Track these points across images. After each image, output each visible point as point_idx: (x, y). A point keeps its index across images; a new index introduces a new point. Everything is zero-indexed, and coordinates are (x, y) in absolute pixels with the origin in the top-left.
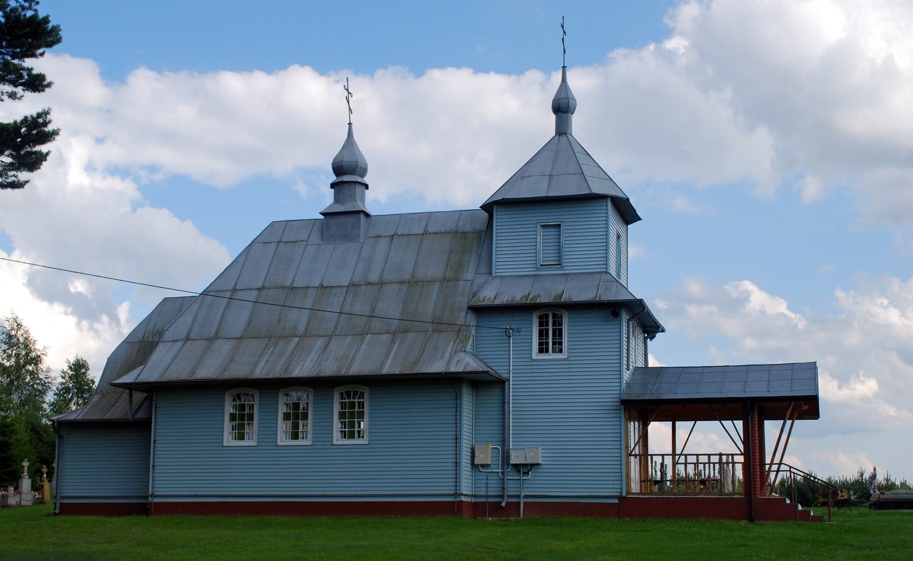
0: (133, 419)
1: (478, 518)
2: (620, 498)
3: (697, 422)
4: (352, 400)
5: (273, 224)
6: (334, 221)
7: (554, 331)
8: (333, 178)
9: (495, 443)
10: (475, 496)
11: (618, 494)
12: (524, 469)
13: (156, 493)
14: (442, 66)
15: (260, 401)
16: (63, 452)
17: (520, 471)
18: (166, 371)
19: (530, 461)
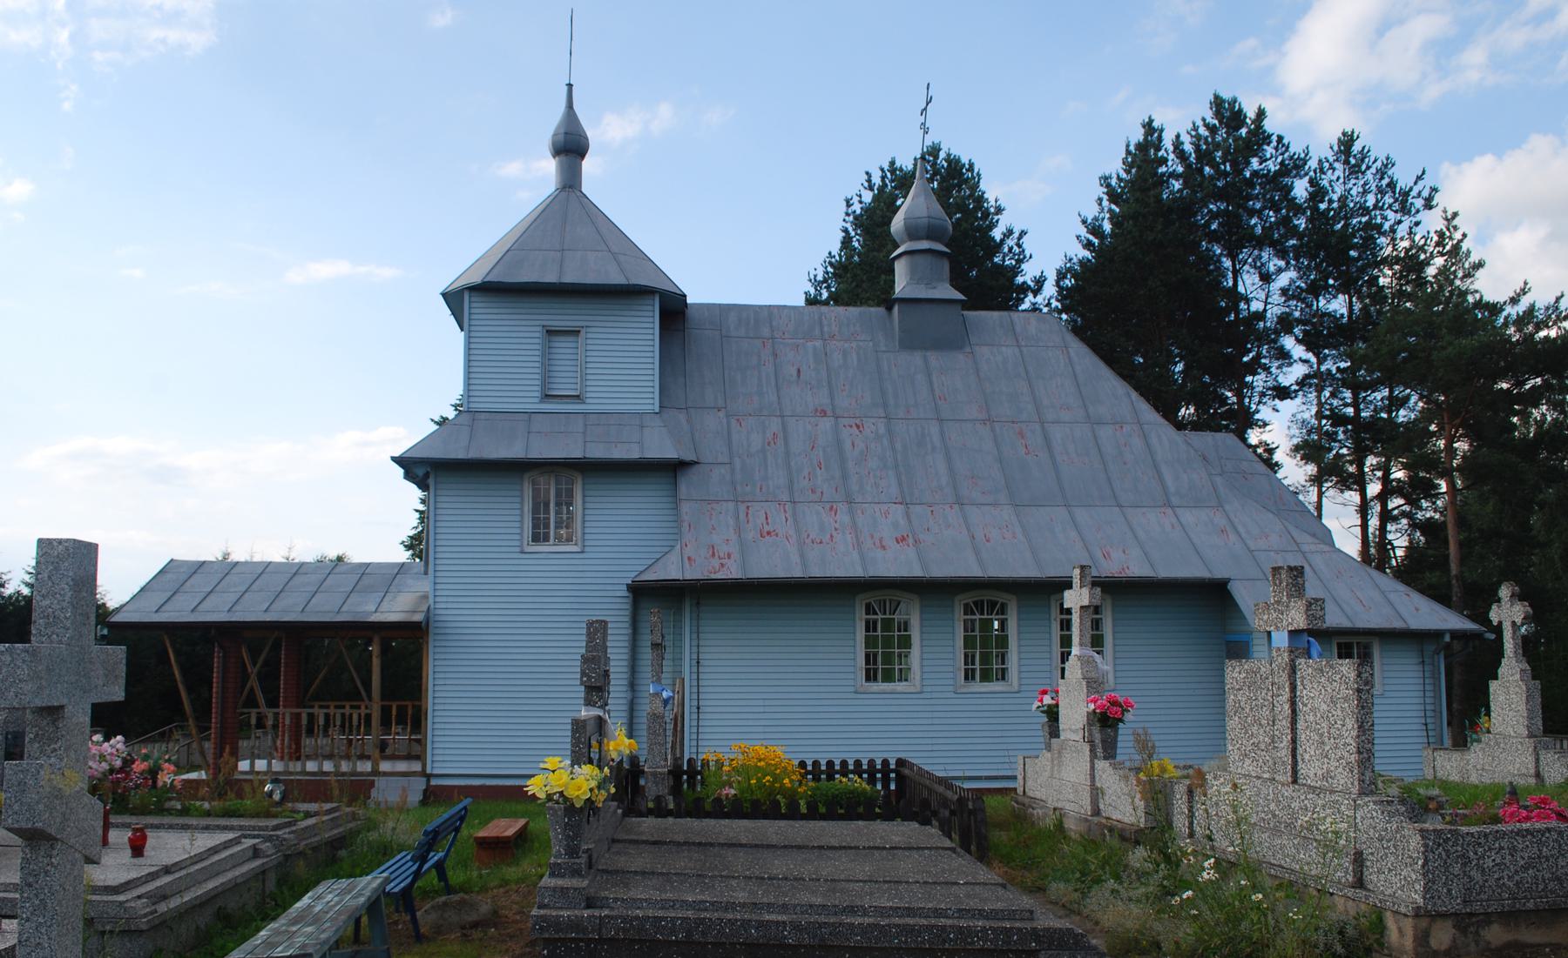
4: (985, 617)
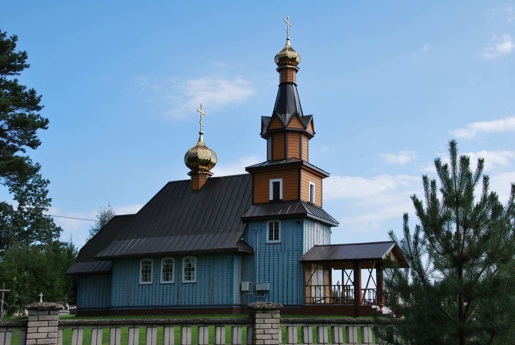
4: (168, 264)
5: (170, 184)
7: (275, 230)
12: (263, 293)
15: (197, 262)
18: (177, 244)
19: (264, 289)
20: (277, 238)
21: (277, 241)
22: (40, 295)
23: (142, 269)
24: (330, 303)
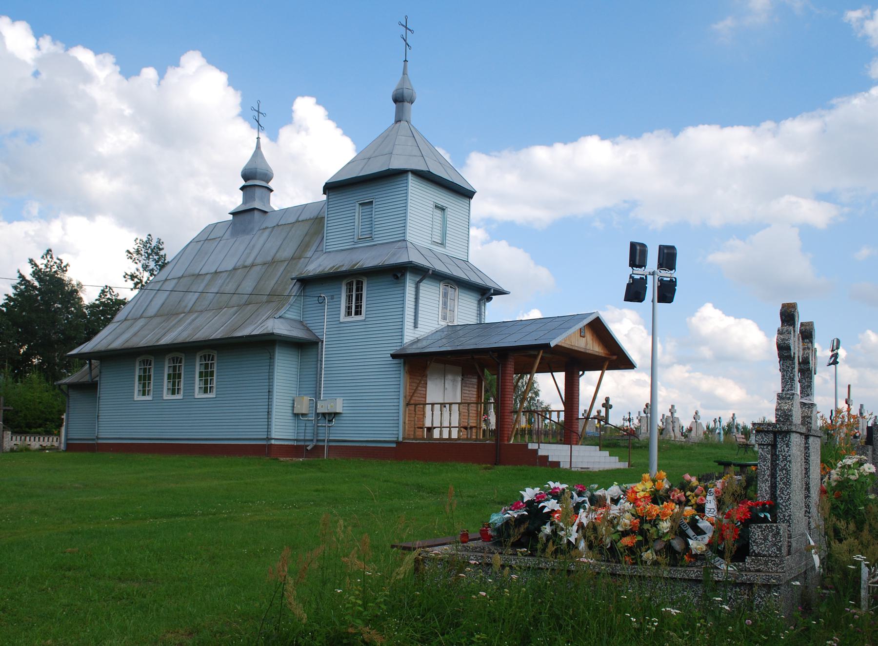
0: (92, 381)
1: (282, 459)
2: (397, 442)
3: (585, 372)
4: (207, 362)
6: (241, 217)
8: (242, 183)
9: (311, 395)
10: (297, 440)
11: (396, 439)
12: (331, 416)
13: (100, 436)
14: (695, 123)
16: (69, 407)
17: (326, 418)
20: (358, 313)
21: (358, 318)
22: (63, 417)
23: (200, 369)
24: (459, 439)
